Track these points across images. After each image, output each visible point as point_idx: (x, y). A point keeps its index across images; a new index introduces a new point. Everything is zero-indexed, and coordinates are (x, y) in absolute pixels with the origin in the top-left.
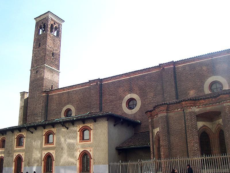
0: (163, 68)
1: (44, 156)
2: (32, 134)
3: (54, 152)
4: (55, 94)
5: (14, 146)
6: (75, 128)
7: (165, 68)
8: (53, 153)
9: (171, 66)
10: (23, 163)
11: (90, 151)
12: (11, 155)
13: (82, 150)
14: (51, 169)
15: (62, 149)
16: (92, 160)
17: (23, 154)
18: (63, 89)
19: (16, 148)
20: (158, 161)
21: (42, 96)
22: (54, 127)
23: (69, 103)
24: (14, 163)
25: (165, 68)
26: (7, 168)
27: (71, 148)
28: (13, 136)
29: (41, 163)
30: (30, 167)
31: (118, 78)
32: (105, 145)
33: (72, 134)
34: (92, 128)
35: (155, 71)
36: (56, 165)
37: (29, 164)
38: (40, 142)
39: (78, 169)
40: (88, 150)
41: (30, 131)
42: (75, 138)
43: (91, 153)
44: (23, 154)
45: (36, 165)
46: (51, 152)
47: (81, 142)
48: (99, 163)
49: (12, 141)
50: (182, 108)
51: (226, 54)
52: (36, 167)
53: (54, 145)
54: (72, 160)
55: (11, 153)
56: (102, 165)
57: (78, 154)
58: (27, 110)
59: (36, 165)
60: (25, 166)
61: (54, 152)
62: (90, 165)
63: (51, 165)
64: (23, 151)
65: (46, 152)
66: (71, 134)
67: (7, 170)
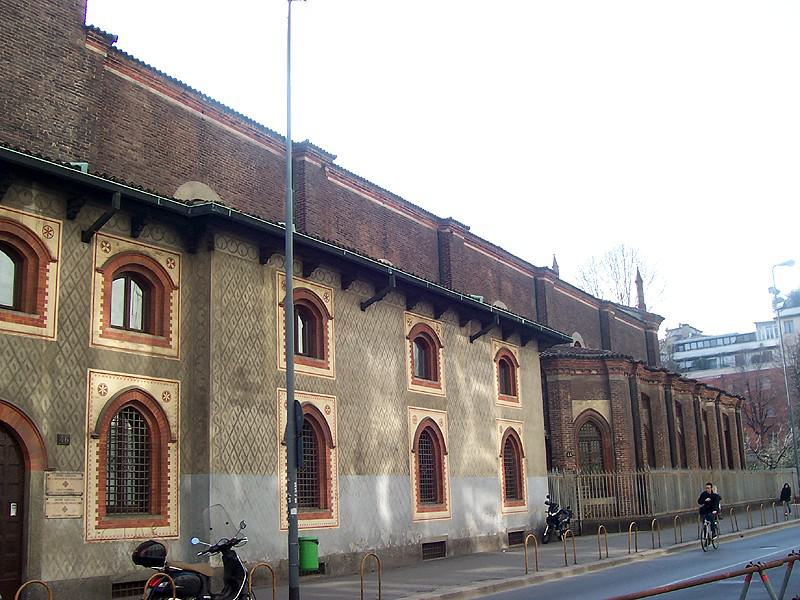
1: (413, 429)
2: (361, 313)
4: (135, 86)
5: (271, 345)
10: (333, 457)
12: (259, 398)
15: (463, 411)
18: (338, 167)
21: (80, 49)
22: (437, 317)
23: (208, 179)
24: (283, 452)
26: (236, 480)
28: (263, 283)
29: (408, 462)
30: (367, 476)
31: (359, 188)
34: (53, 245)
37: (361, 463)
38: (393, 368)
39: (334, 479)
42: (487, 380)
43: (331, 419)
45: (387, 466)
46: (439, 417)
47: (420, 384)
49: (259, 314)
50: (605, 372)
52: (391, 480)
53: (519, 405)
55: (259, 389)
58: (592, 297)
59: (387, 466)
60: (343, 471)
64: (328, 387)
67: (238, 492)
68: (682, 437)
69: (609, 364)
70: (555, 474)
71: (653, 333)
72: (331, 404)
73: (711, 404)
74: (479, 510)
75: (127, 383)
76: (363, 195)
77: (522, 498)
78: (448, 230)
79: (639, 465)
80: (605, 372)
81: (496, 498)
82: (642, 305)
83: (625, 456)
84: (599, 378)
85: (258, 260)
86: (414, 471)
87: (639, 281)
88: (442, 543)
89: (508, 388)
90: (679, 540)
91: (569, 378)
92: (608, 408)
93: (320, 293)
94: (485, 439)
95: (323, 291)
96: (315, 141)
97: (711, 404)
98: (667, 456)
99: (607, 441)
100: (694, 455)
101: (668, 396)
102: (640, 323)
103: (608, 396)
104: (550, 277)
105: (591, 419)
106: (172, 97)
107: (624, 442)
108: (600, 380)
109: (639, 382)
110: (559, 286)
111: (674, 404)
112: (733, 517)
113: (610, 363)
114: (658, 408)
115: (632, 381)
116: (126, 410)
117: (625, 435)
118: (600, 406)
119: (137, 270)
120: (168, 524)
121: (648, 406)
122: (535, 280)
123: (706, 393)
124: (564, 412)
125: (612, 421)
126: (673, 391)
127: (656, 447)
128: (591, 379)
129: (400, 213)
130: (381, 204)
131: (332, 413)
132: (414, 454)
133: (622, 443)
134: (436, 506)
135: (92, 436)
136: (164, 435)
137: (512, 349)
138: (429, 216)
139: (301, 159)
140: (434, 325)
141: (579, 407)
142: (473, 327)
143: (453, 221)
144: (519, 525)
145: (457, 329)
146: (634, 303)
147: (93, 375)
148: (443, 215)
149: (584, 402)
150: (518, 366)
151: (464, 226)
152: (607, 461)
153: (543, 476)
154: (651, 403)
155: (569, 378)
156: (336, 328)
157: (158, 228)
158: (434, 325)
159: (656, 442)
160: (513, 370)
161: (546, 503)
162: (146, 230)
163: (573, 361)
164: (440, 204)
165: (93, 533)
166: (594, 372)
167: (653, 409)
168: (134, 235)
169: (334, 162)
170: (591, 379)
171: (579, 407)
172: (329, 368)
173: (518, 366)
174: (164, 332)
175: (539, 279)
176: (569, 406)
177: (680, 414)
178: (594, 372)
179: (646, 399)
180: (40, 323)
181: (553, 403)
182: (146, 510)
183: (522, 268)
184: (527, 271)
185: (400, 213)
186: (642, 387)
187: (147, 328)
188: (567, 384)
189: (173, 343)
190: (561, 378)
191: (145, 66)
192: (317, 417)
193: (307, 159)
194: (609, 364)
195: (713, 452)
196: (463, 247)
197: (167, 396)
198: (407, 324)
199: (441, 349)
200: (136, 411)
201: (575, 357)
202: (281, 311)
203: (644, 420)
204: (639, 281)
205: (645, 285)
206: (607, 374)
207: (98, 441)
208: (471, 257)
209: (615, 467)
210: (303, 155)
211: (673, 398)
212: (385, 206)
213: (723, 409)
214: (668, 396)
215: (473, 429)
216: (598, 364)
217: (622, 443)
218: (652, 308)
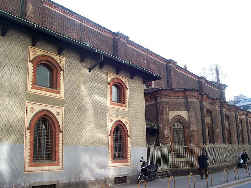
1: (30, 115)
3: (61, 111)
8: (58, 113)
9: (125, 41)
13: (115, 119)
14: (56, 153)
17: (128, 121)
19: (61, 92)
20: (184, 146)
22: (59, 53)
27: (100, 112)
31: (66, 13)
32: (143, 119)
35: (107, 35)
36: (65, 144)
40: (124, 121)
43: (60, 118)
44: (128, 121)
48: (137, 144)
50: (186, 97)
53: (127, 109)
57: (110, 125)
63: (56, 139)
65: (38, 108)
66: (96, 83)
68: (242, 131)
69: (188, 93)
70: (153, 147)
71: (223, 92)
73: (244, 117)
74: (94, 166)
75: (43, 108)
76: (68, 16)
77: (126, 158)
78: (118, 38)
79: (204, 142)
80: (186, 97)
81: (108, 159)
82: (218, 81)
83: (196, 137)
84: (183, 101)
85: (57, 53)
86: (28, 140)
87: (217, 72)
89: (121, 99)
90: (237, 178)
91: (168, 100)
92: (187, 115)
94: (101, 127)
95: (126, 81)
96: (121, 32)
97: (244, 117)
98: (236, 140)
99: (187, 130)
100: (235, 138)
101: (221, 112)
102: (218, 87)
103: (187, 109)
104: (173, 64)
105: (179, 119)
106: (59, 11)
107: (195, 131)
108: (184, 101)
109: (205, 104)
110: (130, 44)
111: (224, 115)
112: (226, 174)
113: (188, 93)
114: (216, 116)
115: (201, 103)
116: (42, 118)
117: (196, 128)
118: (184, 114)
121: (228, 120)
122: (166, 65)
123: (241, 112)
124: (164, 116)
125: (189, 120)
126: (224, 110)
127: (215, 134)
128: (180, 101)
129: (91, 27)
130: (80, 22)
132: (29, 131)
133: (194, 131)
134: (51, 163)
135: (27, 129)
137: (124, 80)
138: (193, 75)
139: (169, 64)
140: (57, 58)
141: (172, 114)
142: (89, 63)
143: (120, 33)
144: (123, 173)
145: (77, 63)
146: (215, 80)
147: (62, 109)
148: (115, 31)
149: (176, 112)
150: (127, 89)
151: (126, 37)
152: (187, 140)
153: (143, 146)
154: (213, 114)
155: (168, 100)
156: (129, 92)
158: (57, 58)
159: (214, 132)
160: (124, 90)
161: (141, 161)
163: (169, 92)
164: (114, 29)
165: (28, 168)
166: (180, 98)
167: (213, 117)
169: (177, 64)
170: (180, 101)
171: (172, 114)
172: (60, 94)
173: (127, 89)
174: (124, 102)
175: (220, 91)
176: (168, 114)
177: (241, 123)
178: (180, 98)
179: (209, 112)
180: (58, 93)
181: (160, 112)
183: (159, 59)
184: (163, 61)
185: (91, 27)
186: (206, 106)
188: (167, 103)
190: (164, 100)
191: (96, 24)
192: (51, 116)
193: (171, 64)
194: (188, 93)
195: (245, 138)
196: (128, 48)
197: (58, 113)
198: (31, 54)
199: (62, 72)
200: (46, 119)
201: (170, 90)
202: (31, 65)
203: (227, 125)
204: (217, 72)
205: (219, 73)
206: (187, 98)
207: (30, 131)
208: (135, 53)
209: (190, 142)
210: (170, 63)
211: (224, 113)
212: (82, 23)
213: (239, 117)
214: (221, 112)
215: (92, 120)
216: (183, 94)
217: (194, 131)
218: (223, 82)
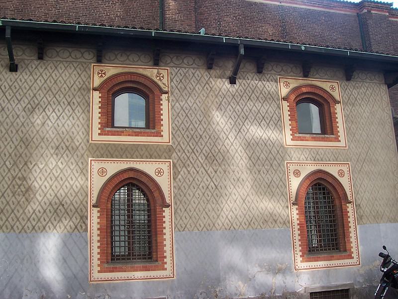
0: (369, 12)
2: (13, 76)
3: (165, 167)
6: (267, 84)
7: (374, 12)
11: (341, 173)
16: (350, 208)
22: (156, 64)
25: (374, 12)
33: (258, 105)
34: (336, 94)
36: (179, 228)
40: (333, 170)
41: (11, 58)
42: (278, 124)
43: (345, 181)
48: (377, 218)
51: (315, 6)
52: (65, 244)
54: (268, 205)
56: (389, 225)
61: (165, 167)
62: (344, 226)
66: (250, 104)
72: (345, 169)
77: (345, 250)
88: (347, 290)
93: (326, 86)
119: (307, 96)
120: (166, 269)
131: (346, 175)
132: (96, 210)
136: (159, 202)
157: (177, 57)
162: (312, 71)
165: (96, 275)
168: (306, 75)
182: (337, 249)
187: (324, 131)
189: (342, 138)
